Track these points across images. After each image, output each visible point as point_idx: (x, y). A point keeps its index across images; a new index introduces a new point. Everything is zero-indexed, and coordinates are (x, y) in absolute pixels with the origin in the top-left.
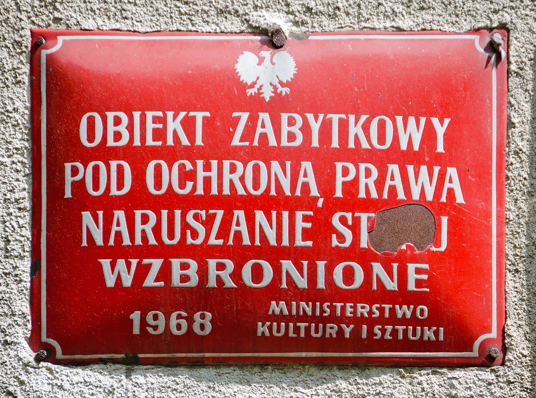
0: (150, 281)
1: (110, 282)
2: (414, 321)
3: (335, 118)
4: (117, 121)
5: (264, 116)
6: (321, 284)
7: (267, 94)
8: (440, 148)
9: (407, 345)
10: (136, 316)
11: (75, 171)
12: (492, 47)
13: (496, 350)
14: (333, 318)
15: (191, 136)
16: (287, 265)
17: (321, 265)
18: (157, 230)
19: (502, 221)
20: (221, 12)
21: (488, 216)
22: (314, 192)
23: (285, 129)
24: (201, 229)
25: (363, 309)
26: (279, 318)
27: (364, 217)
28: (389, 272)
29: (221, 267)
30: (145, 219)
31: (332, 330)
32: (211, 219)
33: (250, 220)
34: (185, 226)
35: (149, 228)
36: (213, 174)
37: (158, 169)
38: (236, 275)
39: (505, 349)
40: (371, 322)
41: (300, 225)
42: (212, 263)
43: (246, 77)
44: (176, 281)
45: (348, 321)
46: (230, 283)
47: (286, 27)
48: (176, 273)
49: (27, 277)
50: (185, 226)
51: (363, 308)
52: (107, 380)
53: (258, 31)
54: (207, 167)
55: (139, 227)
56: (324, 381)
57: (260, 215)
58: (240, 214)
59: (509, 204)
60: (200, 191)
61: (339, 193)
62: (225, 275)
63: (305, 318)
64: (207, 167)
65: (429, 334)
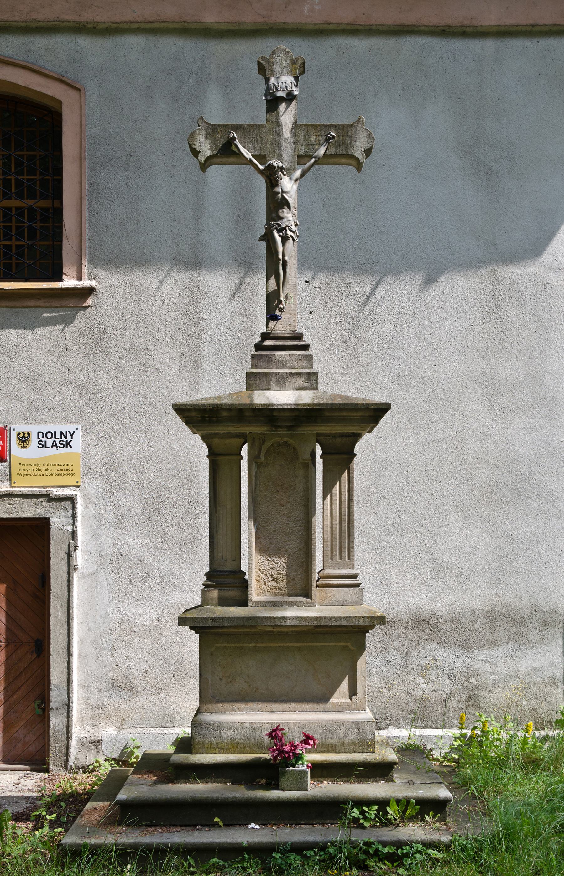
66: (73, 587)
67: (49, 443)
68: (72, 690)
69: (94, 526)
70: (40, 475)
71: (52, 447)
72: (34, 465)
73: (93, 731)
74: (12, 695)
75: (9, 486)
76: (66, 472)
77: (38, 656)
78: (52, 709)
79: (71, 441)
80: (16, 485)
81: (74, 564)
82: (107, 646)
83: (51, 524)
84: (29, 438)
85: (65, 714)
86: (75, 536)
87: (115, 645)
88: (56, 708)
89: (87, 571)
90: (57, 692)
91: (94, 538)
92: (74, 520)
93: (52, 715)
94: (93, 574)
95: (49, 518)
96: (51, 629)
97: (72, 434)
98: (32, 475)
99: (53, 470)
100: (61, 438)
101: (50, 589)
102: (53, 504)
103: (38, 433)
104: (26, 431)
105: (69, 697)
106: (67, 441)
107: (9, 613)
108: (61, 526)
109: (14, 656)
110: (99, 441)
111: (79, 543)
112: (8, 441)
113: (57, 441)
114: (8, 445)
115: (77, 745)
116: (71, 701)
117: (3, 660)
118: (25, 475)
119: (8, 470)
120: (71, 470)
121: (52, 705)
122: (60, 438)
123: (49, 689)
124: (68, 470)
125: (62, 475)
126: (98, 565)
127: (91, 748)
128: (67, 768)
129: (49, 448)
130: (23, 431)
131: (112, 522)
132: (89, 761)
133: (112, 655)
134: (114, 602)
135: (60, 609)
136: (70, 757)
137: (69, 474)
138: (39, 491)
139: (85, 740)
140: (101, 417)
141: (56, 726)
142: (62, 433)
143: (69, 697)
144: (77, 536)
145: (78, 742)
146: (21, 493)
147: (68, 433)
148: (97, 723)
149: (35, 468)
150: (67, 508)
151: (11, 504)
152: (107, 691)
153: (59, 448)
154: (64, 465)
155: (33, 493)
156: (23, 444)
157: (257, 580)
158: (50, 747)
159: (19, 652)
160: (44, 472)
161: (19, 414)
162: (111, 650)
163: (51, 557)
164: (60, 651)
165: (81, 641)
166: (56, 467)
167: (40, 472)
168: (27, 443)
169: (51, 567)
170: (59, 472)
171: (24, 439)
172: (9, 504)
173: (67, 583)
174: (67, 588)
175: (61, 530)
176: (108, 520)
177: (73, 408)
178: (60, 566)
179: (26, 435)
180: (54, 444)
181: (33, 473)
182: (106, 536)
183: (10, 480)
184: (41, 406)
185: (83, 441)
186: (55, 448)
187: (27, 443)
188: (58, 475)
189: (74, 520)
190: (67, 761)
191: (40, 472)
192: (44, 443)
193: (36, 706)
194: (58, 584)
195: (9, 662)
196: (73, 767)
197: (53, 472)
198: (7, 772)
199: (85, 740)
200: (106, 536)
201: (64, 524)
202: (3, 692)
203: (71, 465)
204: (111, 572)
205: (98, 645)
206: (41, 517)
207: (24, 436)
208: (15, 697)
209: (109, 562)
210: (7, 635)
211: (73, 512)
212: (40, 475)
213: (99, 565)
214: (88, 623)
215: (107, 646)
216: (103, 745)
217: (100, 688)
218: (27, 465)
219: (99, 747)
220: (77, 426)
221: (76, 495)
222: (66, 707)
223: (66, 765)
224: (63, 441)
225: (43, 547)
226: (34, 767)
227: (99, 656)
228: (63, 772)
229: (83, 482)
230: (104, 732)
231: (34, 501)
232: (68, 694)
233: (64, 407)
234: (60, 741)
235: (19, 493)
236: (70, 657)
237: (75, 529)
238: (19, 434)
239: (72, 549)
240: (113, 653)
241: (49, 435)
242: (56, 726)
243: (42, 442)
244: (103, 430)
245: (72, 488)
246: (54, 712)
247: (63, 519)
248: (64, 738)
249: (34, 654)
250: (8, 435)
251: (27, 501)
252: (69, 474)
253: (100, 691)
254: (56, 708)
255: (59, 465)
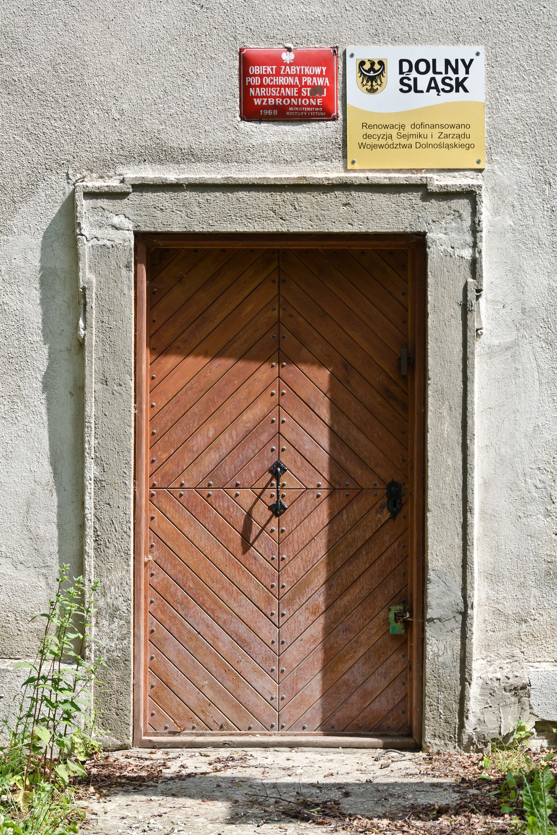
0: (264, 104)
1: (256, 104)
2: (319, 111)
3: (302, 67)
4: (257, 68)
5: (288, 67)
6: (300, 104)
7: (288, 62)
8: (324, 74)
9: (318, 116)
10: (261, 111)
11: (248, 79)
12: (334, 51)
13: (336, 117)
14: (302, 111)
15: (272, 71)
16: (293, 100)
17: (300, 100)
18: (265, 92)
19: (337, 89)
20: (279, 44)
21: (334, 88)
22: (298, 84)
23: (292, 70)
24: (275, 92)
25: (309, 109)
26: (291, 111)
27: (309, 89)
28: (314, 101)
29: (279, 100)
30: (263, 90)
31: (302, 113)
32: (277, 90)
33: (285, 90)
34: (271, 91)
35: (264, 92)
36: (277, 80)
37: (266, 79)
38: (282, 102)
39: (338, 117)
40: (310, 112)
41: (295, 91)
42: (277, 99)
43: (284, 59)
44: (270, 104)
45: (306, 112)
46: (281, 104)
47: (292, 47)
48: (270, 102)
49: (238, 102)
50: (271, 91)
51: (279, 100)
52: (255, 125)
53: (286, 48)
54: (276, 79)
55: (262, 92)
56: (301, 124)
57: (287, 89)
58: (283, 89)
59: (338, 85)
60: (274, 84)
61: (303, 84)
62: (280, 102)
63: (296, 111)
64: (276, 79)
65: (322, 114)
66: (473, 374)
67: (423, 82)
68: (472, 583)
69: (512, 251)
70: (404, 146)
71: (428, 91)
72: (393, 127)
73: (509, 666)
74: (340, 596)
75: (342, 169)
76: (457, 141)
77: (394, 516)
78: (431, 620)
79: (465, 79)
80: (356, 166)
81: (477, 326)
82: (537, 495)
83: (430, 245)
84: (382, 73)
85: (458, 632)
86: (478, 270)
87: (553, 493)
88: (439, 619)
89: (497, 342)
90: (442, 587)
91: (510, 275)
92: (475, 237)
93: (430, 631)
94: (510, 348)
95: (425, 234)
96: (430, 458)
97: (467, 63)
98: (389, 146)
99: (429, 136)
100: (447, 72)
101: (424, 377)
102: (434, 205)
103: (401, 62)
104: (375, 58)
105: (464, 597)
106: (457, 79)
107: (336, 428)
108: (450, 249)
109: (345, 516)
110: (521, 79)
111: (485, 286)
112: (340, 78)
113: (439, 78)
114: (340, 86)
115: (480, 695)
116: (470, 606)
117: (323, 523)
118: (374, 147)
119: (340, 137)
120: (465, 136)
121: (430, 613)
122: (444, 72)
123: (423, 580)
124: (459, 136)
125: (448, 146)
126: (518, 330)
127: (508, 700)
128: (460, 741)
129: (422, 92)
130: (371, 58)
131: (547, 243)
132: (507, 728)
133: (548, 514)
134: (551, 405)
135: (448, 418)
136: (467, 718)
137: (461, 146)
138: (406, 179)
139: (496, 684)
140: (525, 30)
141: (438, 656)
142: (447, 62)
143: (464, 597)
144: (482, 270)
145: (482, 688)
146: (370, 182)
147: (460, 63)
148: (517, 651)
149: (394, 132)
150: (461, 212)
151: (349, 204)
152: (538, 586)
153: (442, 93)
154: (452, 126)
155: (394, 182)
156: (370, 83)
157: (129, 724)
158: (427, 699)
159: (355, 507)
160: (412, 141)
161: (362, 24)
162: (544, 502)
163: (429, 311)
164: (447, 502)
165: (486, 484)
166: (436, 132)
167: (403, 141)
168: (379, 82)
169: (431, 332)
170: (442, 141)
171: (372, 74)
172: (345, 205)
173: (461, 364)
174: (460, 375)
175: (448, 258)
176: (539, 240)
177: (470, 13)
178: (447, 331)
179: (377, 67)
180: (433, 85)
181: (389, 142)
182: (535, 271)
183: (345, 156)
184: (406, 8)
185: (490, 78)
186: (433, 92)
187: (379, 82)
188: (440, 146)
189: (475, 237)
190: (462, 726)
191: (403, 141)
192: (411, 83)
193: (392, 616)
194: (443, 367)
195: (335, 528)
196: (475, 740)
197: (429, 141)
198: (337, 750)
199: (497, 685)
200: (535, 271)
201: (456, 245)
202: (323, 589)
203: (465, 126)
204: (544, 345)
205: (519, 493)
206: (408, 230)
207: (372, 69)
208: (346, 599)
209: (542, 325)
210: (331, 474)
211: (473, 222)
212: (404, 146)
213: (522, 330)
214: (499, 449)
215: (537, 495)
216: (532, 695)
217: (523, 580)
218: (378, 127)
219: (524, 699)
220: (481, 49)
221: (479, 187)
222: (460, 618)
223: (460, 735)
224: (451, 79)
225: (404, 294)
226: (389, 740)
227: (521, 515)
228: (451, 749)
229: (491, 161)
230: (532, 669)
231: (395, 197)
232: (464, 589)
233: (452, 11)
234: (448, 686)
235: (366, 182)
236: (469, 515)
237: (477, 255)
238: (362, 63)
239: (471, 295)
240: (549, 508)
241: (422, 67)
242: (438, 656)
243: (409, 79)
244: (529, 56)
245: (468, 173)
246: (436, 626)
247: (453, 235)
248: (455, 682)
249: (385, 510)
250: (341, 66)
251: (380, 199)
252: (461, 146)
253: (522, 585)
254: (439, 619)
255: (442, 126)
